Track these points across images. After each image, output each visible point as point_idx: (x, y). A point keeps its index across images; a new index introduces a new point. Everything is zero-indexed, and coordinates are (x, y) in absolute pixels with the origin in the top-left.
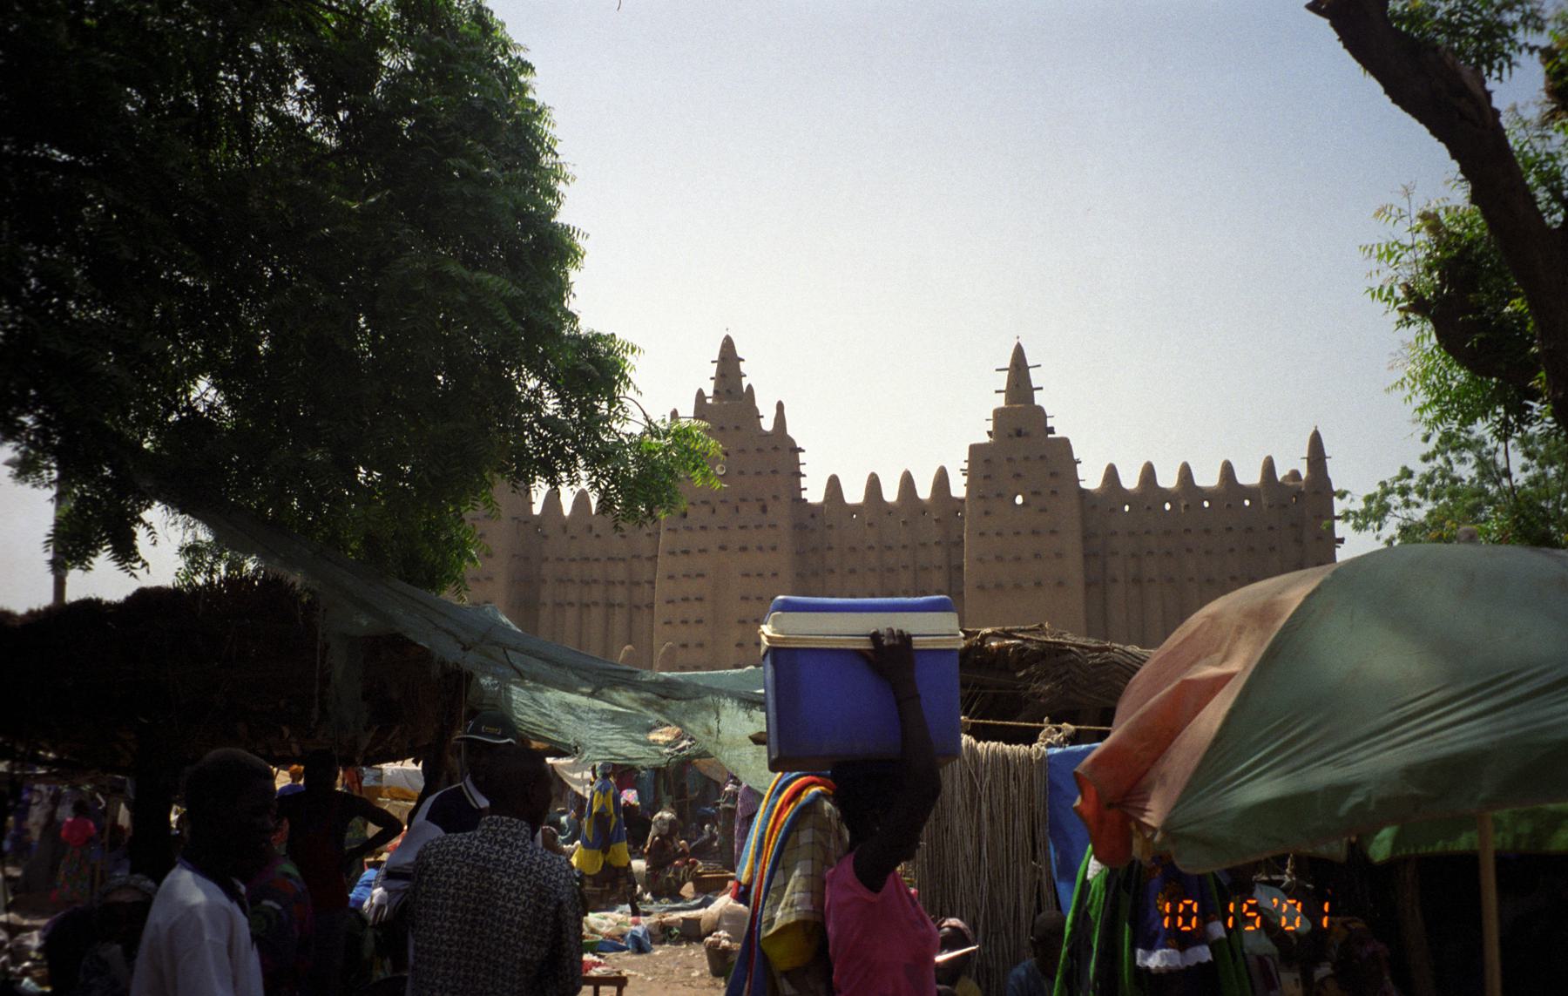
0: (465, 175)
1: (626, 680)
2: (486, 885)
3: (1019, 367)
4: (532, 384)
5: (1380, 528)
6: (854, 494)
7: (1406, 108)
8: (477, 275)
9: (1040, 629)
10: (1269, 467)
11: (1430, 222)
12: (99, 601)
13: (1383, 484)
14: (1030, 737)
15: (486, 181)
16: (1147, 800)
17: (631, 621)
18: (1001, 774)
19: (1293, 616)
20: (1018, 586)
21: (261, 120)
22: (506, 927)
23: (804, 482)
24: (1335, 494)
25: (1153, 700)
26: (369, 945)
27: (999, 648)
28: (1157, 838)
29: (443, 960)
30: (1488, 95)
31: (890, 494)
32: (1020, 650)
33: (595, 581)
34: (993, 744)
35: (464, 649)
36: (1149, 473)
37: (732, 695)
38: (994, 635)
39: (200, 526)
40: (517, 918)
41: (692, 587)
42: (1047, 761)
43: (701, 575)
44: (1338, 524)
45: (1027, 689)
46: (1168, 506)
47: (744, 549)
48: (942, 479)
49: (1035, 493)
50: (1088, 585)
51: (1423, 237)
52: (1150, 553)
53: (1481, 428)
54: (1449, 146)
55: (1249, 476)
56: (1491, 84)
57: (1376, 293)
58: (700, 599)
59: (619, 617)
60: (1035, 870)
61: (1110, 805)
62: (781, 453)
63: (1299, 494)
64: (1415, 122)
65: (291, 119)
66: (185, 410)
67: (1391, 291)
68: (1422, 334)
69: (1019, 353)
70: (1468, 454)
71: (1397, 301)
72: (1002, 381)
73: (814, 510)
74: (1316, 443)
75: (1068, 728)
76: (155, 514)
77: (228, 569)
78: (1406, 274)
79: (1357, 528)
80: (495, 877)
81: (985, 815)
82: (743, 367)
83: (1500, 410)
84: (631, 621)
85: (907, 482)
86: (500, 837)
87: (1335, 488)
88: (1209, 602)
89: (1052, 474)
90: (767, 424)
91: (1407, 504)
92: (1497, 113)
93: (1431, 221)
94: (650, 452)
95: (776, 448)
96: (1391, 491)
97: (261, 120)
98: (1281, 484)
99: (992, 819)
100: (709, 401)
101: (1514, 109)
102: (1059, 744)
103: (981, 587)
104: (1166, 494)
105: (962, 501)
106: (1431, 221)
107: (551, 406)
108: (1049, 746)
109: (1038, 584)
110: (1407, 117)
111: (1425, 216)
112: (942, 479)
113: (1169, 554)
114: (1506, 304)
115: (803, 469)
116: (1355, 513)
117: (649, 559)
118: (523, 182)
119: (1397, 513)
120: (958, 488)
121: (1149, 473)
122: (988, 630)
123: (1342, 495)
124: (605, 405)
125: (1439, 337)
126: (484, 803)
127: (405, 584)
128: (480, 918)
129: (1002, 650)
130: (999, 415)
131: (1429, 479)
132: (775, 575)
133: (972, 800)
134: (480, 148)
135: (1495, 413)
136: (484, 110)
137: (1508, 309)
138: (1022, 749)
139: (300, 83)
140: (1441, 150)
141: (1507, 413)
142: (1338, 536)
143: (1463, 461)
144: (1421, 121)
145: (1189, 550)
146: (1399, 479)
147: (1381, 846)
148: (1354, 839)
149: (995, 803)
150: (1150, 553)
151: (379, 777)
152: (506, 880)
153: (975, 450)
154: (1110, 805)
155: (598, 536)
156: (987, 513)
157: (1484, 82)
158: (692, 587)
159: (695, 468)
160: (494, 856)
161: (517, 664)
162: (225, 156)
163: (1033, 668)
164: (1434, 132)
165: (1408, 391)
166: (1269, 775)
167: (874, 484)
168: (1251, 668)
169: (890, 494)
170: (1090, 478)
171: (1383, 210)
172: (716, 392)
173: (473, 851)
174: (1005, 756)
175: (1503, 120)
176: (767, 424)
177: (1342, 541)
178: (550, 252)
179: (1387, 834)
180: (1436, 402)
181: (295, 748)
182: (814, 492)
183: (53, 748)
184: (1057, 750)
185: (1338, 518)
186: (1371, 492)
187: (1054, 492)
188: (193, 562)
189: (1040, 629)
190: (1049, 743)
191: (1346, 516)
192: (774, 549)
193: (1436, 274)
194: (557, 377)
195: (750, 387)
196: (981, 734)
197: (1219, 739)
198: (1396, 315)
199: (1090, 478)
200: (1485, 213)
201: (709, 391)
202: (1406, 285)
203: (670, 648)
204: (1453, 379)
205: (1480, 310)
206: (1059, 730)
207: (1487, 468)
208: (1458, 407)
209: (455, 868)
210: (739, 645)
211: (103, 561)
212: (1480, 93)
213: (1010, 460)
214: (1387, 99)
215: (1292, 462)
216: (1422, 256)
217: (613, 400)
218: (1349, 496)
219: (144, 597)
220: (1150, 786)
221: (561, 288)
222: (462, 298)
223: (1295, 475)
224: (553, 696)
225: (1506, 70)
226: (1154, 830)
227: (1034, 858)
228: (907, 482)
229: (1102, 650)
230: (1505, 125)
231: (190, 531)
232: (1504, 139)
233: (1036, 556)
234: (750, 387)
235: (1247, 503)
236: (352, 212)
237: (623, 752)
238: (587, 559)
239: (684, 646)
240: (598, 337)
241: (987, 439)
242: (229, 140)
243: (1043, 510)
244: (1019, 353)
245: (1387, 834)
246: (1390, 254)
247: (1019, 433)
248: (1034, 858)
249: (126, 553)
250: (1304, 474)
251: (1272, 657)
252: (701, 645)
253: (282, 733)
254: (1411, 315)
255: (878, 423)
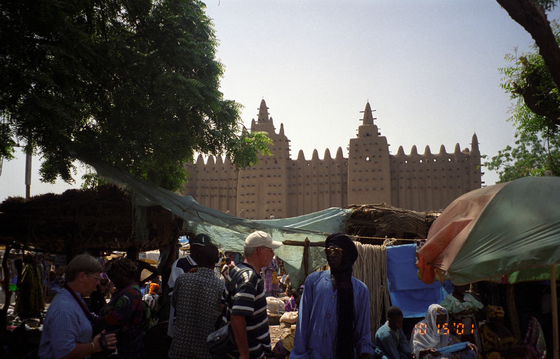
0: (183, 44)
1: (240, 222)
2: (201, 290)
3: (368, 111)
4: (207, 118)
5: (498, 169)
6: (308, 157)
7: (517, 21)
8: (189, 80)
9: (383, 205)
10: (458, 147)
11: (523, 61)
12: (53, 194)
13: (500, 152)
14: (380, 243)
15: (192, 46)
16: (442, 262)
17: (228, 202)
18: (370, 255)
19: (492, 200)
20: (367, 190)
21: (109, 24)
22: (208, 305)
23: (290, 152)
24: (482, 157)
25: (441, 230)
26: (149, 314)
27: (368, 212)
28: (446, 274)
29: (187, 315)
30: (546, 16)
31: (321, 157)
32: (375, 212)
33: (216, 188)
34: (368, 245)
35: (184, 211)
36: (414, 149)
37: (276, 228)
38: (366, 207)
39: (91, 167)
40: (212, 302)
41: (251, 190)
42: (386, 251)
43: (253, 186)
44: (482, 167)
45: (378, 226)
46: (421, 161)
47: (269, 176)
48: (340, 151)
49: (374, 157)
50: (392, 189)
51: (521, 65)
52: (415, 178)
53: (539, 135)
54: (532, 34)
55: (450, 150)
56: (547, 12)
57: (503, 86)
58: (253, 194)
59: (224, 201)
60: (382, 288)
61: (428, 264)
62: (282, 142)
63: (468, 157)
64: (520, 25)
65: (119, 23)
66: (85, 127)
67: (509, 85)
68: (519, 102)
69: (368, 106)
70: (531, 142)
71: (511, 89)
72: (362, 116)
73: (294, 163)
74: (475, 138)
75: (394, 239)
76: (76, 163)
77: (99, 183)
78: (514, 79)
79: (490, 169)
80: (204, 288)
81: (365, 270)
82: (269, 111)
83: (547, 128)
84: (228, 202)
85: (328, 152)
86: (205, 275)
87: (481, 155)
88: (458, 197)
89: (380, 150)
90: (277, 132)
91: (508, 160)
92: (549, 23)
93: (524, 60)
94: (248, 143)
95: (280, 140)
96: (502, 156)
97: (109, 24)
98: (462, 153)
99: (367, 271)
100: (256, 123)
101: (554, 21)
102: (391, 245)
103: (354, 190)
104: (420, 157)
105: (347, 159)
106: (524, 60)
107: (213, 126)
108: (387, 245)
109: (374, 189)
110: (517, 23)
111: (521, 59)
112: (340, 151)
113: (421, 178)
114: (550, 91)
115: (290, 148)
116: (489, 163)
117: (235, 180)
118: (204, 45)
119: (504, 163)
120: (346, 155)
121: (414, 149)
122: (364, 206)
123: (484, 157)
124: (231, 126)
125: (525, 101)
126: (195, 264)
127: (162, 189)
128: (199, 302)
129: (369, 213)
130: (360, 128)
131: (517, 151)
132: (280, 186)
133: (360, 264)
134: (189, 34)
135: (545, 129)
136: (189, 21)
137: (551, 92)
138: (378, 247)
139: (123, 11)
140: (529, 35)
141: (549, 128)
142: (482, 172)
143: (529, 144)
144: (522, 25)
145: (429, 177)
146: (506, 150)
147: (513, 278)
148: (503, 276)
149: (368, 265)
150: (415, 178)
151: (145, 256)
152: (208, 289)
153: (352, 141)
154: (428, 264)
155: (208, 172)
156: (356, 164)
157: (544, 12)
158: (251, 190)
159: (262, 148)
160: (204, 281)
161: (202, 217)
162: (97, 36)
163: (380, 219)
164: (526, 29)
165: (514, 122)
166: (486, 253)
167: (315, 153)
168: (478, 217)
169: (321, 157)
170: (393, 151)
171: (507, 55)
172: (259, 120)
173: (197, 279)
174: (372, 249)
175: (551, 25)
176: (277, 132)
177: (483, 173)
178: (212, 71)
179: (515, 274)
180: (524, 125)
181: (119, 245)
182: (294, 156)
183: (34, 245)
184: (390, 247)
185: (483, 165)
186: (495, 156)
187: (380, 156)
188: (87, 181)
189: (383, 205)
190: (387, 244)
191: (486, 164)
192: (280, 176)
193: (525, 79)
194: (215, 116)
195: (271, 118)
196: (363, 241)
197: (467, 242)
198: (510, 94)
199: (393, 151)
200: (544, 57)
201: (256, 119)
202: (514, 83)
203: (243, 212)
204: (530, 117)
205: (540, 92)
206: (391, 240)
207: (538, 148)
208: (532, 127)
209: (191, 285)
210: (267, 210)
211: (59, 179)
212: (543, 16)
213: (364, 144)
214: (510, 17)
215: (466, 145)
216: (520, 73)
217: (234, 124)
218: (487, 157)
219: (70, 193)
220: (443, 257)
221: (215, 84)
222: (184, 88)
223: (467, 150)
224: (213, 227)
225: (552, 8)
226: (445, 271)
227: (382, 284)
228: (328, 152)
229: (404, 212)
230: (552, 27)
231: (88, 169)
232: (551, 32)
233: (374, 179)
234: (271, 118)
235: (450, 160)
236: (144, 57)
237: (236, 248)
238: (213, 180)
239: (247, 211)
240: (229, 102)
241: (356, 137)
242: (98, 31)
243: (376, 163)
244: (368, 106)
245: (515, 274)
246: (509, 72)
247: (368, 135)
248: (382, 284)
249: (66, 177)
250: (470, 150)
251: (484, 215)
252: (253, 210)
253: (114, 240)
254: (515, 94)
255: (317, 131)
